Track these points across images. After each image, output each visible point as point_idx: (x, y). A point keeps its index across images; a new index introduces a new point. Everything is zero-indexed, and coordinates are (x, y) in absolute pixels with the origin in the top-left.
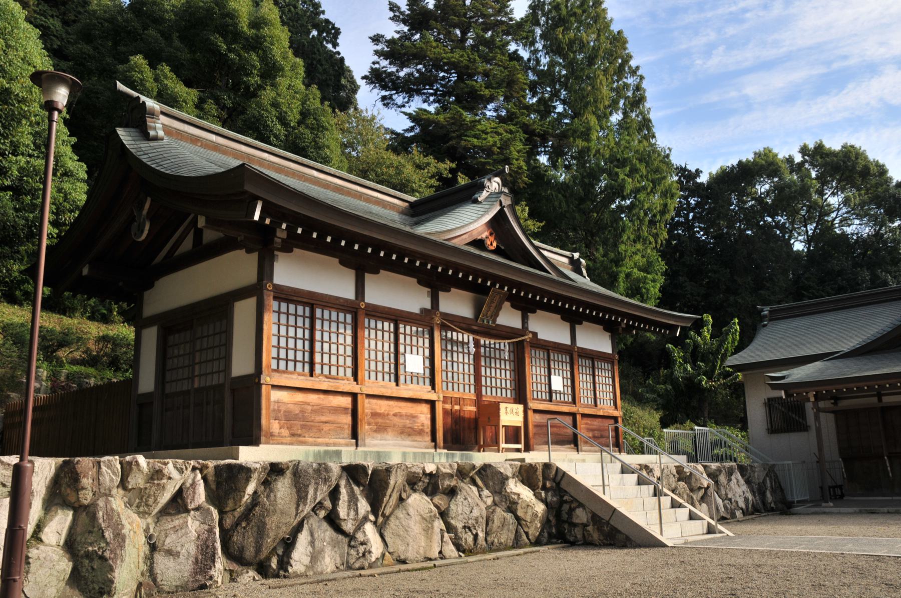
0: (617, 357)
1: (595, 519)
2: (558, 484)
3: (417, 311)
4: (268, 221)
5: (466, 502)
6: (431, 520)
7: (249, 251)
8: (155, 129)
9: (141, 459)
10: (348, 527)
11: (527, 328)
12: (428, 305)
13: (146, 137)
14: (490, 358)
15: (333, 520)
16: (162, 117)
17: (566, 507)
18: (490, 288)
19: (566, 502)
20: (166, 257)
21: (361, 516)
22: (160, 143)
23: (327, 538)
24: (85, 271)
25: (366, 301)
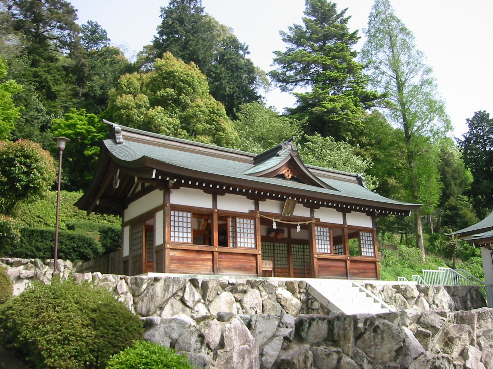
0: (375, 229)
1: (322, 306)
2: (307, 291)
3: (247, 212)
4: (160, 178)
5: (251, 297)
6: (232, 304)
7: (161, 190)
8: (119, 139)
9: (99, 274)
10: (190, 304)
11: (314, 217)
12: (253, 208)
13: (117, 143)
14: (321, 236)
15: (183, 301)
16: (123, 133)
17: (310, 301)
18: (286, 199)
19: (310, 299)
20: (132, 193)
21: (196, 300)
22: (122, 145)
23: (180, 308)
24: (98, 203)
25: (218, 208)
